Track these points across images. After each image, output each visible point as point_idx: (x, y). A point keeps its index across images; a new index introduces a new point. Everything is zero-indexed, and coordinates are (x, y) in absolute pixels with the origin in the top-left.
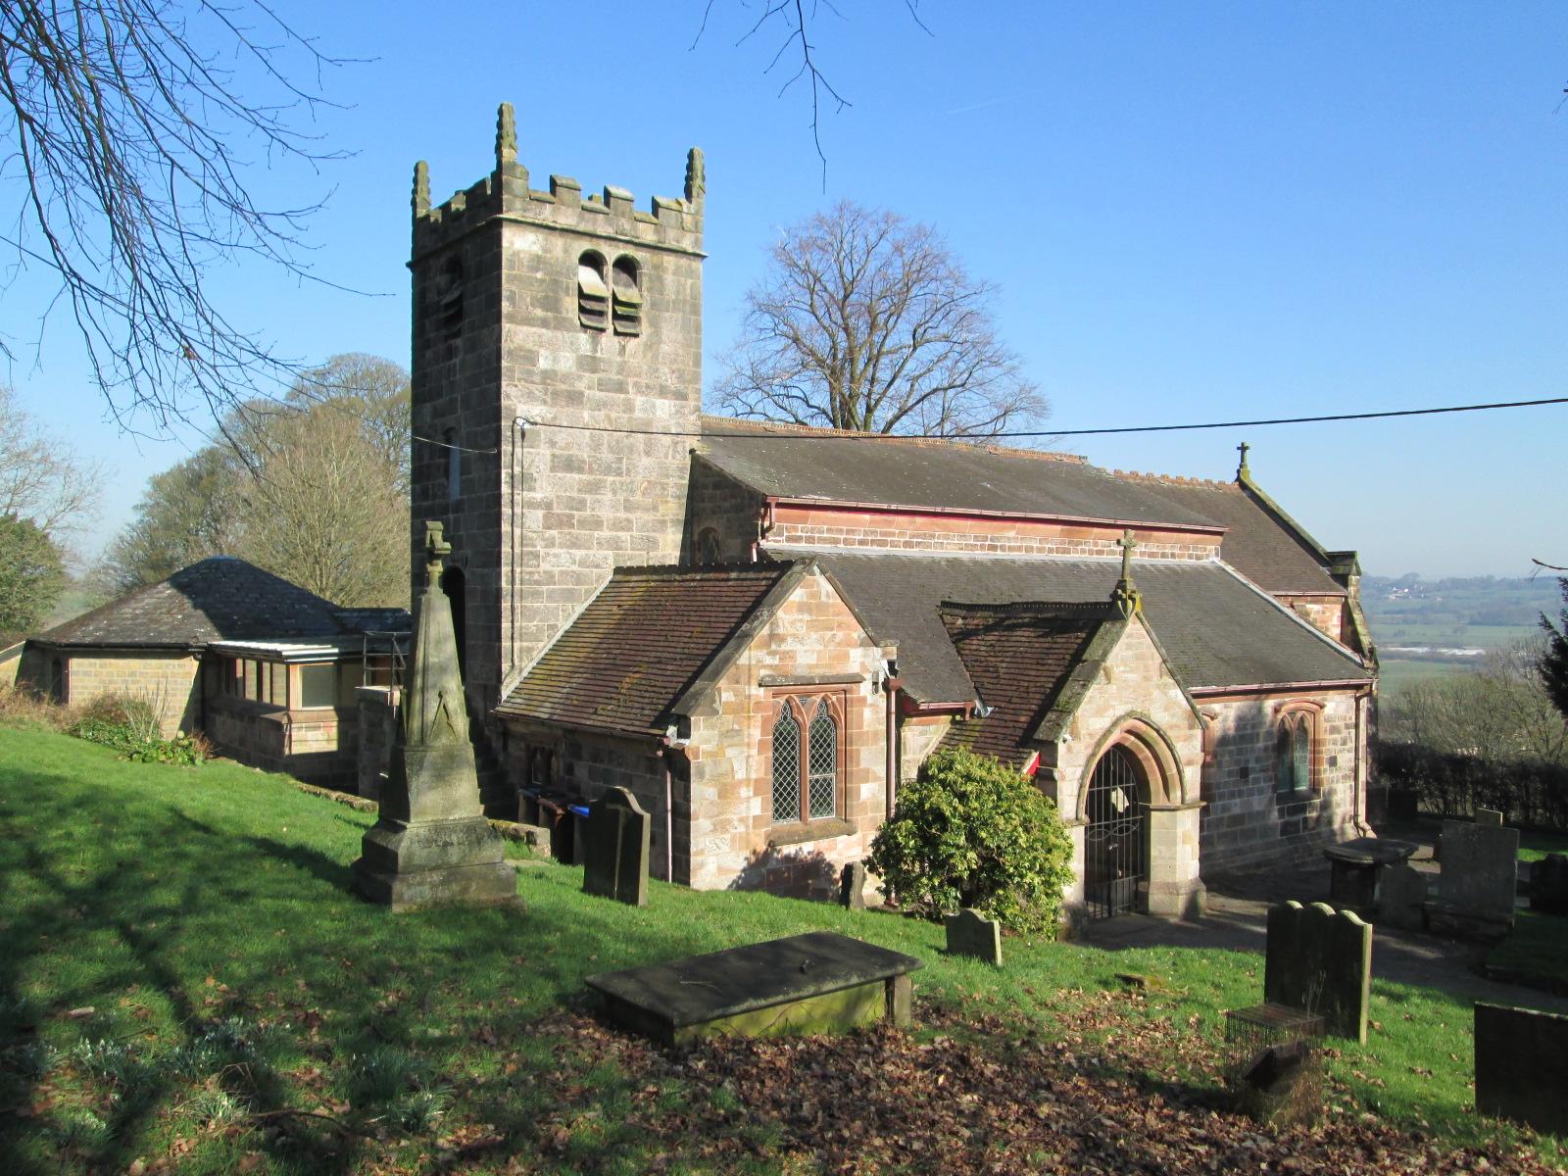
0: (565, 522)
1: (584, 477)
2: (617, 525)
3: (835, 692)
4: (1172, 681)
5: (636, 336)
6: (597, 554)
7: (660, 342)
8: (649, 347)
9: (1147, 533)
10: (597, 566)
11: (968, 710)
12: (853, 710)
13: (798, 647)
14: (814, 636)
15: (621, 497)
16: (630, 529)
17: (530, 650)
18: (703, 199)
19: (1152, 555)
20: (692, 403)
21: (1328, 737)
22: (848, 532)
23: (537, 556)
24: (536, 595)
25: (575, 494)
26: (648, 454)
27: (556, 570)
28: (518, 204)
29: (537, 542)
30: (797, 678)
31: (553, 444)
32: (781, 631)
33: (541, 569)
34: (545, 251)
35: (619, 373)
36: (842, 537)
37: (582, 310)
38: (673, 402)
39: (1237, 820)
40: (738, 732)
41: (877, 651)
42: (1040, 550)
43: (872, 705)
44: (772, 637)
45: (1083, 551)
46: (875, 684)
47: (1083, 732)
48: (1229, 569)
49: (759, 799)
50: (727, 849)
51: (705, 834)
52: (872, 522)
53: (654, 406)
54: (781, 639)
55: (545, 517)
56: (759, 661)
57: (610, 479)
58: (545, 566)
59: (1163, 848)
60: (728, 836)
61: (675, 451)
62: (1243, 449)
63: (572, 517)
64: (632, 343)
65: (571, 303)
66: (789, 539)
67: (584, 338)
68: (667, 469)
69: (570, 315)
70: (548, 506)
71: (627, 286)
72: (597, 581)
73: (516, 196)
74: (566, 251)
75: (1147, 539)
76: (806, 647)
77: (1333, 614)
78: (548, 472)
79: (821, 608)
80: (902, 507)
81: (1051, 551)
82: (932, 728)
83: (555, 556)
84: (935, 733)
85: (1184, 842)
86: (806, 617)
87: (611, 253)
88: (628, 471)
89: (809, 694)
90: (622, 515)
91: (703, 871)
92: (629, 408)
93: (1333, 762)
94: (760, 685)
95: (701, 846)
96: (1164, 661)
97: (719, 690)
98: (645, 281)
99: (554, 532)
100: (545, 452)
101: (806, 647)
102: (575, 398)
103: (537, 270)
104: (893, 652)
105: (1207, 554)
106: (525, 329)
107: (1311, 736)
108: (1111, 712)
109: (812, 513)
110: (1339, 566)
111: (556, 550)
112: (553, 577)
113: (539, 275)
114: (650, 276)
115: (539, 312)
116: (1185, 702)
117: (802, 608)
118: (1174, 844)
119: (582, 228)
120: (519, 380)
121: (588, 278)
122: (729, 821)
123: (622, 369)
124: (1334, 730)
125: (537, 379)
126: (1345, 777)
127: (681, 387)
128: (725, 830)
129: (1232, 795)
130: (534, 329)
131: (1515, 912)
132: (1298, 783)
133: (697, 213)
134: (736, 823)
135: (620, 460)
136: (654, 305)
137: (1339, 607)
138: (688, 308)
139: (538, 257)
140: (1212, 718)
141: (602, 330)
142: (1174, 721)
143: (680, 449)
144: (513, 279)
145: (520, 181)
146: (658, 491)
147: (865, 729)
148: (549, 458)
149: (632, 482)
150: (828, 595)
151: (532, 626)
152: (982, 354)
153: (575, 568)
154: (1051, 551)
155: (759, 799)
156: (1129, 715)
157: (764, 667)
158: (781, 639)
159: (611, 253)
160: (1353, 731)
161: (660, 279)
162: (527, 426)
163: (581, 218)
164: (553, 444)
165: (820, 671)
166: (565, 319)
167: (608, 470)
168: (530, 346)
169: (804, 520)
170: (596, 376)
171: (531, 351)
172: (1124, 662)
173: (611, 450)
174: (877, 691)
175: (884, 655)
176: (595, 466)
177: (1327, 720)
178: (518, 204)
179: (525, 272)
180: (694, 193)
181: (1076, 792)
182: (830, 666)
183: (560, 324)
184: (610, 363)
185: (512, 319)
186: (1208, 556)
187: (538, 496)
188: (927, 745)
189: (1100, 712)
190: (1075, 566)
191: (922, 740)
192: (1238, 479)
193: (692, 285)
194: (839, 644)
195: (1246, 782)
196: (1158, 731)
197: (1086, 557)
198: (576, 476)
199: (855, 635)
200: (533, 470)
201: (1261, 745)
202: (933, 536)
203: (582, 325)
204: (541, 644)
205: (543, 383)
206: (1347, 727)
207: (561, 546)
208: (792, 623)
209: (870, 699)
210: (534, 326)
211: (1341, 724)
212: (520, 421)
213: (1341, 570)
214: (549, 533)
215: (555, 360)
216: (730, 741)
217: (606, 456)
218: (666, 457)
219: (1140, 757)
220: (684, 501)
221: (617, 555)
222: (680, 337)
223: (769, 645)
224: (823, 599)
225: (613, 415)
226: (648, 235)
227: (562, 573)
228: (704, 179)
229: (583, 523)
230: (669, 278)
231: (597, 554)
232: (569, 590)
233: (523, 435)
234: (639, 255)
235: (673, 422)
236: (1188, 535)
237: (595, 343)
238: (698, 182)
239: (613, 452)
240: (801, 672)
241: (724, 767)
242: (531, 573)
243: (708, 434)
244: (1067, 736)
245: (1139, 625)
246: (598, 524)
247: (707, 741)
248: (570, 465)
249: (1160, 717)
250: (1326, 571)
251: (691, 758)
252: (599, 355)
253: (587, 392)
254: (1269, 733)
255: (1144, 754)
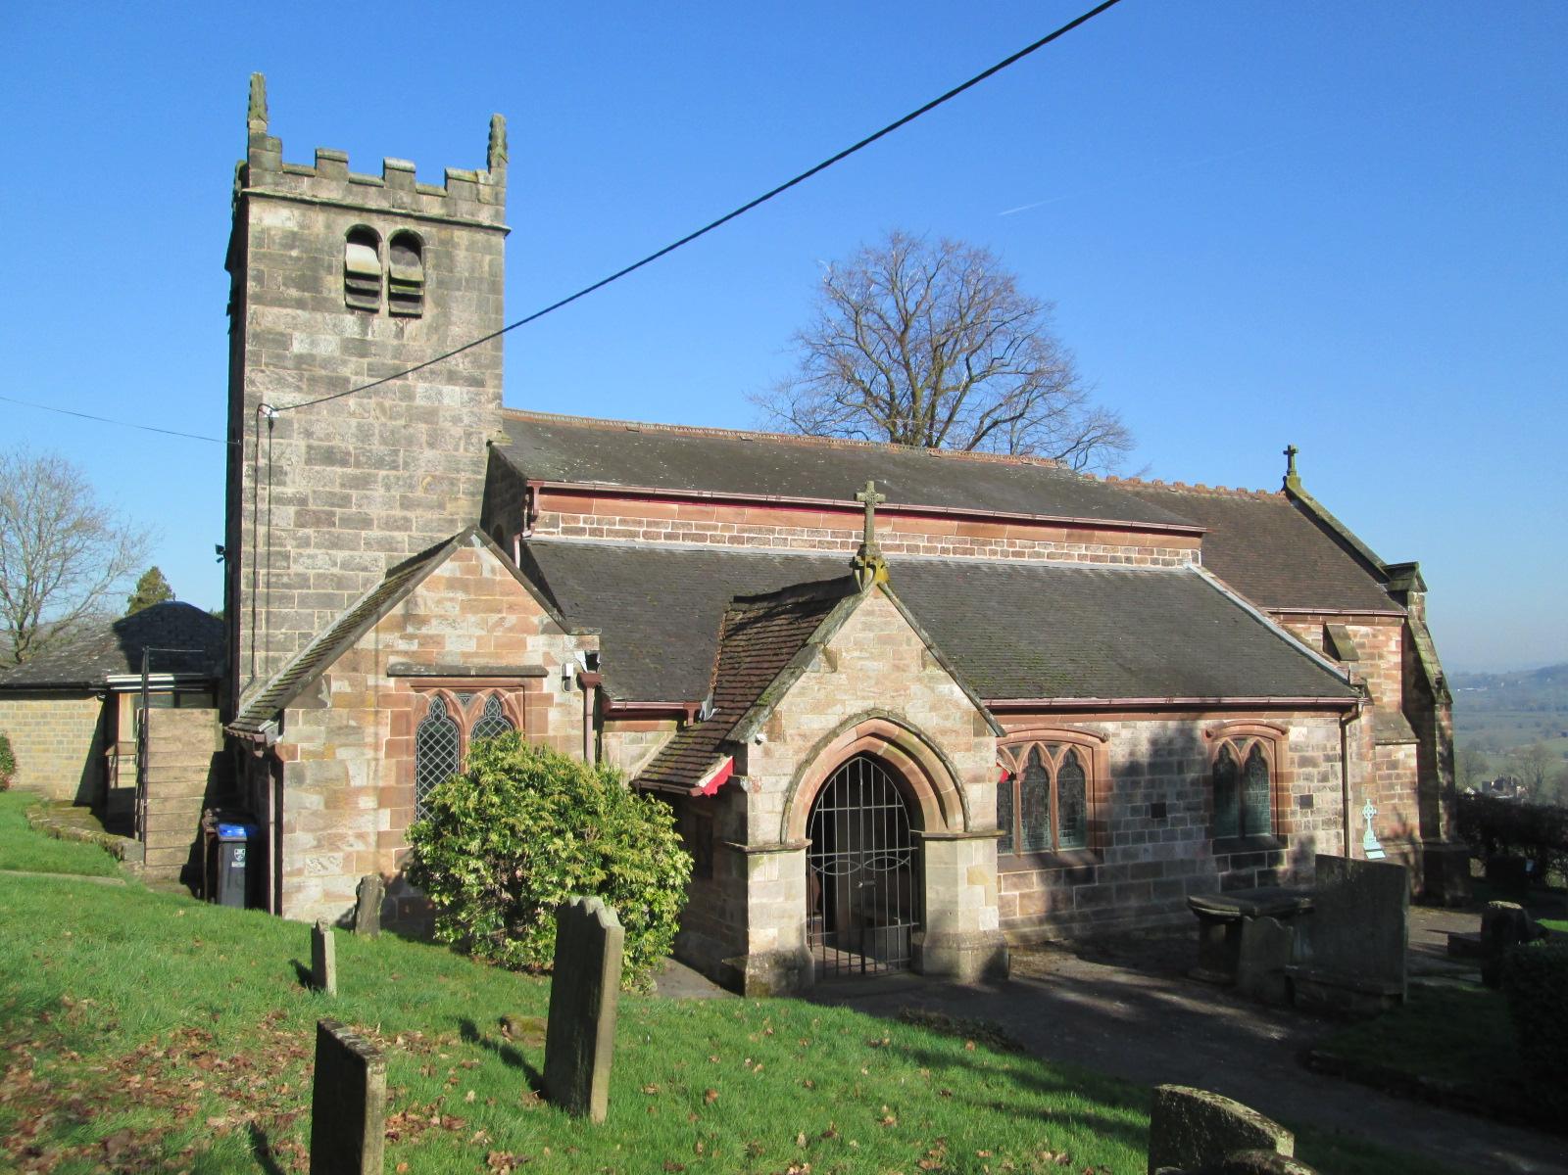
0: (323, 520)
1: (349, 471)
2: (390, 524)
3: (511, 688)
4: (942, 673)
5: (418, 316)
6: (365, 556)
7: (448, 323)
8: (434, 328)
9: (1086, 532)
10: (365, 569)
11: (691, 712)
12: (534, 709)
13: (448, 631)
14: (472, 618)
15: (396, 493)
16: (407, 529)
17: (276, 660)
18: (504, 171)
19: (1095, 559)
20: (490, 390)
21: (1296, 770)
22: (649, 524)
23: (286, 557)
24: (285, 600)
25: (337, 490)
26: (431, 445)
27: (311, 573)
28: (269, 178)
29: (287, 542)
30: (443, 667)
31: (308, 434)
32: (421, 611)
33: (292, 571)
34: (302, 227)
35: (394, 357)
36: (642, 530)
37: (349, 290)
38: (465, 389)
39: (1155, 869)
40: (357, 730)
41: (570, 641)
42: (928, 550)
43: (560, 705)
44: (408, 617)
45: (994, 552)
46: (566, 678)
47: (789, 732)
48: (1208, 576)
49: (387, 812)
50: (338, 870)
51: (305, 851)
52: (681, 513)
53: (440, 393)
54: (422, 621)
55: (298, 514)
56: (387, 646)
57: (383, 473)
58: (295, 568)
59: (941, 889)
60: (339, 855)
61: (468, 443)
62: (1290, 453)
63: (333, 514)
64: (414, 324)
65: (335, 285)
66: (566, 531)
67: (350, 321)
68: (457, 462)
69: (333, 295)
70: (302, 501)
71: (412, 264)
72: (364, 585)
73: (266, 170)
74: (328, 227)
75: (1089, 540)
76: (459, 632)
77: (1389, 639)
78: (302, 465)
79: (484, 585)
80: (717, 495)
81: (944, 551)
82: (650, 735)
83: (309, 556)
84: (655, 741)
85: (971, 881)
86: (460, 596)
87: (386, 229)
88: (406, 465)
89: (473, 690)
90: (398, 513)
91: (301, 896)
92: (408, 395)
93: (1306, 802)
94: (389, 676)
95: (298, 865)
96: (929, 648)
97: (328, 679)
98: (429, 259)
99: (310, 531)
100: (299, 443)
101: (459, 632)
102: (339, 387)
103: (292, 247)
104: (594, 642)
105: (1185, 560)
106: (276, 310)
107: (1271, 769)
108: (838, 708)
109: (596, 502)
110: (1398, 582)
111: (311, 551)
112: (308, 579)
113: (294, 253)
114: (436, 252)
115: (294, 293)
116: (966, 701)
117: (452, 584)
118: (955, 882)
119: (348, 201)
120: (267, 365)
121: (360, 257)
122: (342, 837)
123: (398, 352)
124: (1305, 762)
125: (289, 364)
126: (1328, 823)
127: (476, 373)
128: (336, 848)
129: (1139, 838)
130: (289, 311)
131: (1407, 980)
132: (1258, 829)
133: (497, 184)
134: (352, 839)
135: (396, 452)
136: (441, 283)
137: (1398, 630)
138: (485, 286)
139: (294, 235)
140: (1103, 741)
141: (375, 311)
142: (949, 724)
143: (474, 440)
144: (259, 258)
145: (271, 154)
146: (445, 486)
147: (551, 733)
148: (303, 449)
149: (411, 477)
150: (493, 570)
151: (280, 634)
152: (1044, 381)
153: (336, 570)
154: (944, 551)
155: (387, 812)
156: (869, 714)
157: (397, 653)
158: (422, 621)
159: (386, 229)
160: (1338, 765)
161: (450, 256)
162: (275, 415)
163: (349, 192)
164: (308, 434)
165: (482, 661)
166: (326, 300)
167: (380, 463)
168: (281, 328)
169: (587, 510)
170: (365, 361)
171: (282, 334)
172: (859, 645)
173: (384, 441)
174: (567, 688)
175: (580, 645)
176: (363, 459)
177: (1295, 748)
178: (269, 178)
179: (276, 250)
180: (494, 163)
181: (780, 808)
182: (497, 655)
183: (320, 304)
184: (384, 346)
185: (259, 299)
186: (1181, 562)
187: (289, 491)
188: (642, 756)
189: (819, 708)
190: (976, 568)
191: (635, 749)
192: (1285, 488)
193: (491, 261)
194: (511, 629)
195: (1164, 822)
196: (918, 736)
197: (997, 559)
198: (339, 470)
199: (535, 620)
200: (283, 462)
201: (1191, 776)
202: (773, 531)
203: (348, 306)
204: (290, 655)
205: (298, 368)
206: (1328, 759)
207: (318, 546)
208: (439, 602)
209: (557, 698)
210: (286, 306)
211: (1319, 755)
212: (267, 410)
213: (1399, 585)
214: (302, 532)
215: (313, 343)
216: (343, 740)
217: (377, 447)
218: (457, 450)
219: (903, 769)
220: (480, 498)
221: (391, 557)
222: (475, 318)
223: (404, 628)
224: (486, 574)
225: (387, 403)
226: (434, 209)
227: (319, 576)
228: (505, 147)
229: (346, 522)
230: (461, 255)
231: (365, 556)
232: (328, 596)
233: (271, 423)
234: (422, 230)
235: (465, 410)
236: (1149, 536)
237: (364, 326)
238: (499, 150)
239: (386, 444)
240: (449, 661)
241: (335, 771)
242: (278, 575)
243: (510, 424)
244: (762, 737)
245: (885, 600)
246: (366, 522)
247: (309, 739)
248: (330, 457)
249: (921, 716)
250: (1382, 587)
251: (283, 757)
252: (369, 337)
253: (353, 378)
254: (1204, 762)
255: (908, 766)
